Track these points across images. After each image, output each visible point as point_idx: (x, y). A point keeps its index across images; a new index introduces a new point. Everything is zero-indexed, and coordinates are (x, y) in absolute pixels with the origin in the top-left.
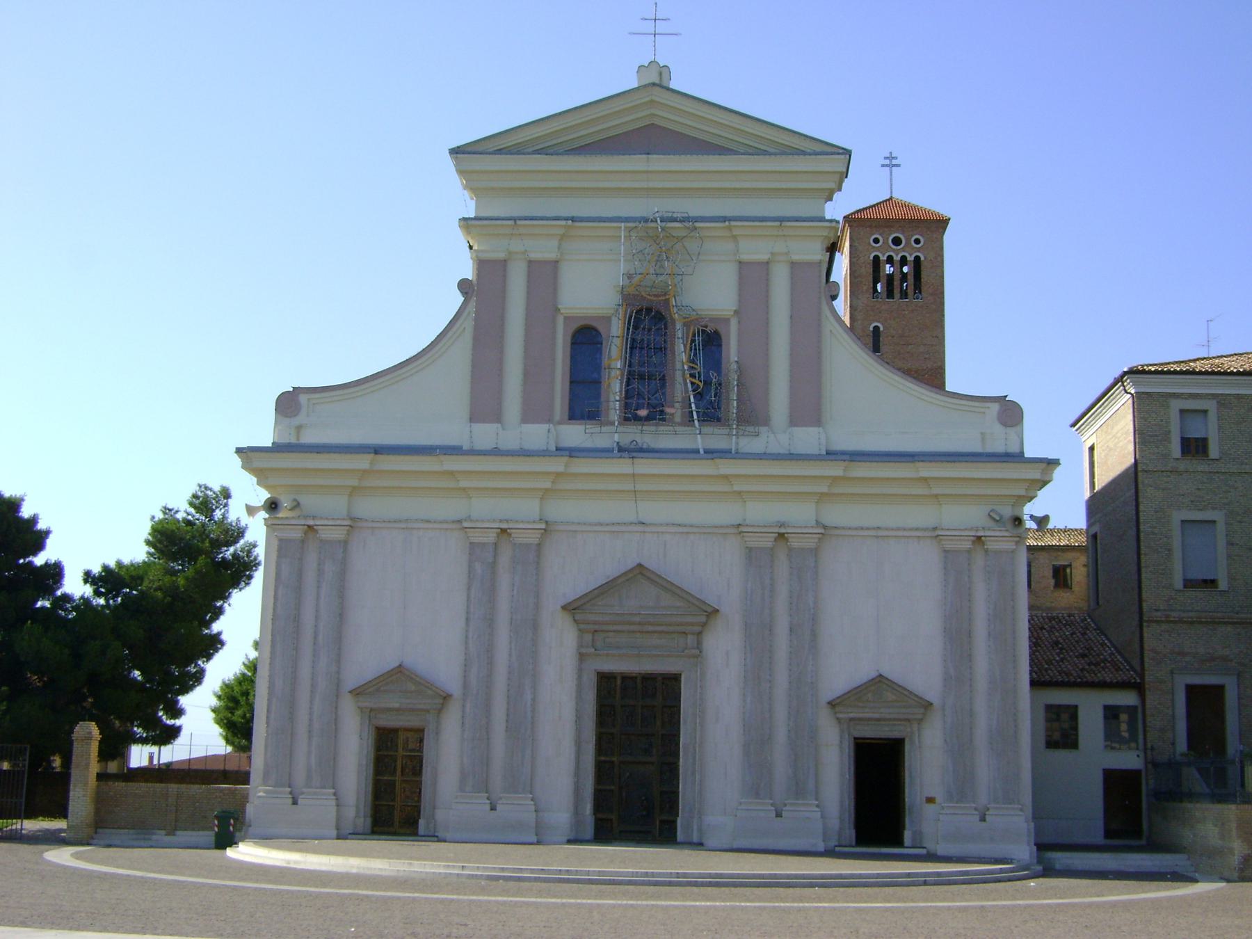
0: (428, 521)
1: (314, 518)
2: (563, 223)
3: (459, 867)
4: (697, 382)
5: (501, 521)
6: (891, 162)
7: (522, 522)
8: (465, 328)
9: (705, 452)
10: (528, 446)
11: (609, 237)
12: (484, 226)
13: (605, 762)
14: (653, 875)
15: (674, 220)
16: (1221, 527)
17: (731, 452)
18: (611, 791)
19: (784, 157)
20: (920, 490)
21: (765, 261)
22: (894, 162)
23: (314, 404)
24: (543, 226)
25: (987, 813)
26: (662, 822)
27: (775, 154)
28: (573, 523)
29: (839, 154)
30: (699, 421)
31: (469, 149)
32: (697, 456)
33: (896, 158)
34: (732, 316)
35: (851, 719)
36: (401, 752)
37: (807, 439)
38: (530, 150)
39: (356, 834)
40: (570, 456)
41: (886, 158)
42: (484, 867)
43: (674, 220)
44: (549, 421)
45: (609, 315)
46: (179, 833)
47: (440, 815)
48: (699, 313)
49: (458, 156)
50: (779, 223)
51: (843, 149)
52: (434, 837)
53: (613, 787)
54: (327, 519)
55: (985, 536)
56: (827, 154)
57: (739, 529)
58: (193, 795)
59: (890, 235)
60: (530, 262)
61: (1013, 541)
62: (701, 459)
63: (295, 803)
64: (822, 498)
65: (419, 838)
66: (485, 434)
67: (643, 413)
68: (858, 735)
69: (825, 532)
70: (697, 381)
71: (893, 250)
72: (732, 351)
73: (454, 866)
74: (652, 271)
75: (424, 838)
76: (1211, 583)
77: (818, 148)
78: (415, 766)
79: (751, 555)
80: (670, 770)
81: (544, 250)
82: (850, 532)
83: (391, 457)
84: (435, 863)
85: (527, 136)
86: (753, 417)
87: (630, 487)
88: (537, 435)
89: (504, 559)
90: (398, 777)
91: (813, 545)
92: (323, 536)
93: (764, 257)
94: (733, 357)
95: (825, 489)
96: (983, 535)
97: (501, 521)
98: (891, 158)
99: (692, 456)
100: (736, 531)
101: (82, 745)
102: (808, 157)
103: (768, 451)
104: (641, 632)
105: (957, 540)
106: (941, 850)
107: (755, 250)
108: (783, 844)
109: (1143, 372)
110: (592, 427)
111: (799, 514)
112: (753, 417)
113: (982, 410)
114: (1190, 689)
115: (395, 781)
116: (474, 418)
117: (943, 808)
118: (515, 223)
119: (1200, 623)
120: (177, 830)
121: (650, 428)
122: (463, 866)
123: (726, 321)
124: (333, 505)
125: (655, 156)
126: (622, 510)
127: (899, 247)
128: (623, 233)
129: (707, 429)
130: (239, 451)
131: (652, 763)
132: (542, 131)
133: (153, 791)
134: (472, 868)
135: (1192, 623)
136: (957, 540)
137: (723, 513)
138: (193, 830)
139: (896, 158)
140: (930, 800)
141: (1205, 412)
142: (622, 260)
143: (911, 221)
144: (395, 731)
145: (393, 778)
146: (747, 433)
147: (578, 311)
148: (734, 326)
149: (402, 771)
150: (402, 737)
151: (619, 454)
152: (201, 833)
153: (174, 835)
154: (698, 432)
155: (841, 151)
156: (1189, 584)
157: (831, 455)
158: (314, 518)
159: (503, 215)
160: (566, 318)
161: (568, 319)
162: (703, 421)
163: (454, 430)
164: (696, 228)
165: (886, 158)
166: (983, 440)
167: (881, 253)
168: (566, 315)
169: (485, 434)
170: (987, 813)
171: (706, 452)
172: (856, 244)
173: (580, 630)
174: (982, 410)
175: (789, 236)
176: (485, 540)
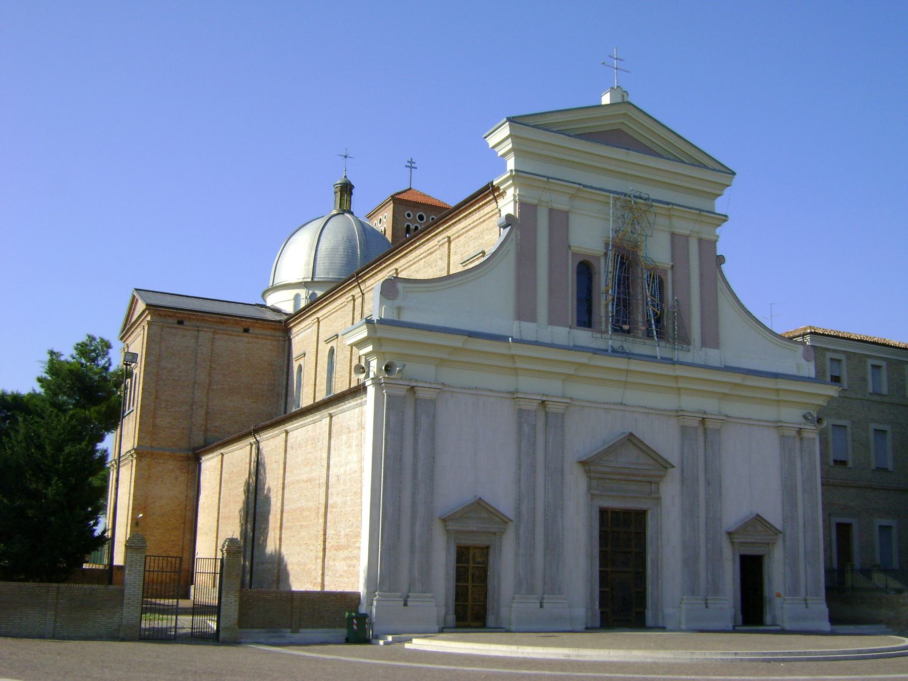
1: (416, 381)
2: (577, 186)
3: (733, 653)
4: (656, 310)
5: (543, 395)
9: (661, 359)
12: (528, 178)
14: (810, 653)
15: (641, 198)
16: (849, 430)
17: (657, 358)
19: (699, 168)
22: (413, 165)
23: (407, 291)
26: (637, 613)
30: (657, 337)
31: (518, 120)
35: (741, 543)
36: (471, 565)
39: (589, 629)
40: (594, 353)
41: (409, 162)
42: (751, 653)
43: (641, 198)
45: (599, 256)
46: (301, 630)
47: (504, 612)
49: (513, 124)
50: (698, 212)
51: (732, 171)
54: (426, 382)
56: (724, 172)
59: (418, 212)
61: (815, 433)
62: (658, 362)
66: (529, 330)
71: (419, 223)
73: (728, 653)
74: (629, 230)
76: (843, 463)
77: (717, 167)
79: (684, 429)
80: (640, 577)
81: (561, 203)
83: (477, 340)
84: (713, 652)
87: (623, 378)
88: (561, 334)
90: (470, 584)
93: (687, 232)
97: (543, 395)
98: (411, 162)
100: (675, 414)
102: (708, 170)
103: (695, 362)
105: (790, 430)
106: (787, 626)
108: (711, 626)
112: (684, 340)
115: (468, 586)
120: (301, 628)
122: (735, 653)
126: (613, 394)
127: (422, 222)
132: (562, 118)
133: (280, 596)
134: (699, 655)
137: (668, 401)
140: (779, 595)
142: (611, 220)
143: (431, 206)
144: (467, 548)
145: (466, 584)
146: (684, 349)
147: (577, 249)
148: (669, 273)
150: (471, 552)
153: (298, 632)
155: (730, 172)
156: (835, 461)
160: (573, 254)
162: (660, 338)
164: (652, 206)
165: (409, 162)
167: (411, 224)
171: (662, 358)
172: (397, 215)
173: (590, 478)
175: (703, 222)
176: (530, 408)
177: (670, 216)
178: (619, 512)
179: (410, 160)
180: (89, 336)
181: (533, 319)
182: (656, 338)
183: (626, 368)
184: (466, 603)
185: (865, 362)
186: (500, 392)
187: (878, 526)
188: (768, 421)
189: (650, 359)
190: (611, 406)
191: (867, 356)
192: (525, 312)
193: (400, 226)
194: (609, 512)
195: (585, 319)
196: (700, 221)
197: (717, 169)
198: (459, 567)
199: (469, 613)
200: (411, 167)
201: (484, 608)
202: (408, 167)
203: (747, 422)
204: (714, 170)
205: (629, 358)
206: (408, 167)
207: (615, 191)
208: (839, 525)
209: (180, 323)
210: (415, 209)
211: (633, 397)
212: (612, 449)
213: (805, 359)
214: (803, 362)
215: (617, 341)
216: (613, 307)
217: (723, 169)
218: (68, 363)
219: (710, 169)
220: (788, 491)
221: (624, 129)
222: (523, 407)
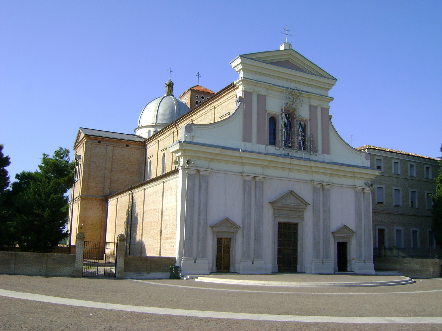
0: (232, 172)
1: (200, 168)
2: (270, 85)
5: (254, 174)
7: (203, 168)
8: (240, 112)
10: (261, 151)
11: (278, 91)
13: (219, 247)
14: (366, 283)
15: (297, 90)
16: (384, 189)
18: (281, 257)
20: (288, 167)
21: (251, 92)
22: (199, 75)
24: (278, 88)
25: (254, 261)
27: (317, 76)
28: (270, 176)
29: (335, 80)
30: (303, 150)
31: (245, 56)
32: (281, 156)
33: (200, 74)
34: (280, 114)
37: (327, 158)
38: (260, 60)
39: (273, 273)
40: (276, 156)
41: (197, 74)
42: (341, 283)
43: (297, 90)
47: (237, 265)
48: (303, 118)
51: (335, 79)
52: (235, 273)
53: (281, 256)
55: (256, 176)
56: (332, 79)
58: (156, 260)
59: (201, 95)
60: (265, 96)
62: (303, 160)
63: (195, 263)
64: (211, 160)
65: (230, 273)
66: (248, 146)
68: (339, 241)
69: (211, 171)
70: (303, 138)
73: (332, 283)
74: (292, 104)
75: (232, 273)
78: (228, 250)
79: (314, 189)
81: (263, 92)
82: (336, 185)
83: (227, 150)
85: (321, 73)
86: (314, 151)
88: (262, 148)
90: (223, 254)
91: (262, 181)
92: (202, 174)
93: (316, 105)
95: (267, 164)
96: (255, 176)
97: (254, 174)
98: (199, 74)
100: (353, 187)
101: (122, 242)
104: (289, 210)
107: (314, 103)
108: (325, 272)
112: (314, 151)
113: (361, 155)
114: (379, 229)
117: (356, 261)
118: (257, 82)
119: (380, 213)
122: (335, 283)
123: (307, 121)
124: (203, 164)
125: (293, 70)
126: (284, 174)
128: (284, 91)
131: (290, 249)
136: (326, 185)
137: (307, 177)
138: (156, 272)
140: (353, 259)
144: (222, 239)
145: (221, 254)
148: (309, 122)
152: (159, 273)
153: (150, 274)
154: (303, 153)
155: (335, 79)
156: (378, 203)
158: (200, 168)
159: (255, 79)
162: (304, 150)
163: (238, 143)
165: (197, 74)
166: (363, 163)
168: (268, 112)
169: (248, 146)
170: (254, 261)
171: (305, 158)
174: (361, 155)
176: (249, 179)
177: (309, 98)
179: (198, 73)
181: (250, 141)
188: (350, 186)
190: (284, 179)
191: (393, 158)
192: (247, 138)
195: (273, 141)
197: (329, 78)
200: (198, 76)
201: (229, 264)
202: (197, 76)
205: (291, 158)
206: (197, 76)
209: (99, 142)
212: (283, 197)
214: (365, 160)
221: (290, 60)
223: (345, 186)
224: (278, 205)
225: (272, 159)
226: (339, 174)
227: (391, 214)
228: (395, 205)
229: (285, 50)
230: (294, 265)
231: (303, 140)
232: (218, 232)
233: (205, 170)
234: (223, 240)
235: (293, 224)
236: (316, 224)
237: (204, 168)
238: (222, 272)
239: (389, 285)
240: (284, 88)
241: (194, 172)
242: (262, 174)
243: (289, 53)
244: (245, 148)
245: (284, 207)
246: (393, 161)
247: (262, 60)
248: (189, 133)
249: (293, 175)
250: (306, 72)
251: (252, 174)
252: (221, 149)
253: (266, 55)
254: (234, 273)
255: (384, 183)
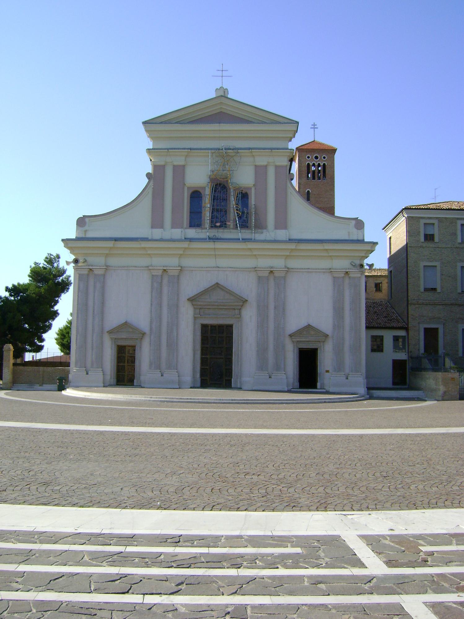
1: (92, 266)
2: (187, 150)
4: (239, 212)
5: (164, 266)
6: (314, 127)
9: (242, 240)
15: (230, 149)
16: (438, 268)
20: (213, 253)
22: (315, 127)
31: (150, 122)
33: (316, 125)
35: (298, 341)
36: (127, 354)
37: (282, 234)
39: (110, 385)
40: (190, 241)
41: (312, 125)
43: (230, 149)
44: (182, 228)
46: (44, 385)
47: (142, 378)
49: (146, 124)
51: (295, 121)
57: (255, 269)
62: (240, 242)
63: (87, 374)
66: (157, 233)
67: (218, 224)
71: (315, 161)
72: (252, 201)
75: (136, 387)
77: (286, 121)
78: (132, 360)
79: (259, 278)
80: (229, 361)
81: (179, 161)
86: (260, 226)
88: (177, 233)
89: (165, 281)
90: (126, 364)
93: (265, 163)
94: (253, 203)
97: (164, 266)
98: (314, 125)
99: (237, 241)
102: (281, 124)
106: (331, 390)
107: (261, 161)
109: (410, 209)
110: (199, 230)
111: (278, 263)
112: (260, 226)
113: (348, 223)
116: (153, 227)
117: (332, 374)
119: (430, 304)
121: (221, 230)
123: (250, 189)
124: (98, 261)
126: (210, 262)
127: (319, 159)
129: (243, 231)
130: (63, 240)
131: (222, 358)
135: (427, 304)
137: (249, 263)
139: (316, 125)
140: (327, 371)
141: (434, 224)
149: (127, 361)
150: (127, 349)
151: (209, 241)
155: (295, 122)
156: (426, 290)
157: (291, 241)
158: (92, 266)
161: (188, 188)
162: (241, 227)
163: (145, 231)
164: (238, 152)
165: (312, 125)
169: (157, 233)
171: (242, 239)
174: (348, 223)
176: (158, 274)
177: (253, 156)
178: (216, 326)
179: (313, 124)
180: (48, 254)
181: (162, 226)
182: (239, 228)
183: (214, 247)
184: (124, 374)
185: (456, 223)
186: (142, 267)
187: (461, 329)
188: (323, 269)
189: (235, 241)
190: (210, 269)
191: (458, 219)
193: (303, 165)
194: (209, 326)
196: (273, 155)
197: (286, 122)
198: (203, 358)
199: (126, 379)
200: (314, 128)
201: (133, 376)
202: (313, 128)
203: (307, 270)
204: (285, 123)
205: (214, 242)
206: (313, 128)
207: (206, 148)
208: (426, 330)
210: (312, 153)
211: (223, 262)
213: (356, 229)
215: (214, 233)
216: (210, 214)
217: (292, 122)
218: (45, 268)
219: (282, 123)
220: (338, 311)
221: (223, 111)
222: (154, 274)
223: (315, 270)
224: (199, 303)
225: (187, 246)
226: (297, 254)
227: (452, 304)
228: (462, 292)
229: (218, 97)
230: (227, 378)
231: (239, 214)
232: (115, 339)
233: (98, 268)
234: (127, 348)
235: (226, 326)
236: (262, 324)
237: (97, 266)
238: (125, 385)
239: (247, 403)
240: (210, 151)
241: (85, 272)
242: (178, 265)
243: (219, 102)
244: (152, 236)
245: (209, 305)
246: (422, 222)
247: (176, 121)
248: (81, 227)
249: (223, 262)
250: (254, 123)
251: (161, 266)
252: (113, 242)
253: (183, 113)
254: (138, 387)
255: (440, 258)
